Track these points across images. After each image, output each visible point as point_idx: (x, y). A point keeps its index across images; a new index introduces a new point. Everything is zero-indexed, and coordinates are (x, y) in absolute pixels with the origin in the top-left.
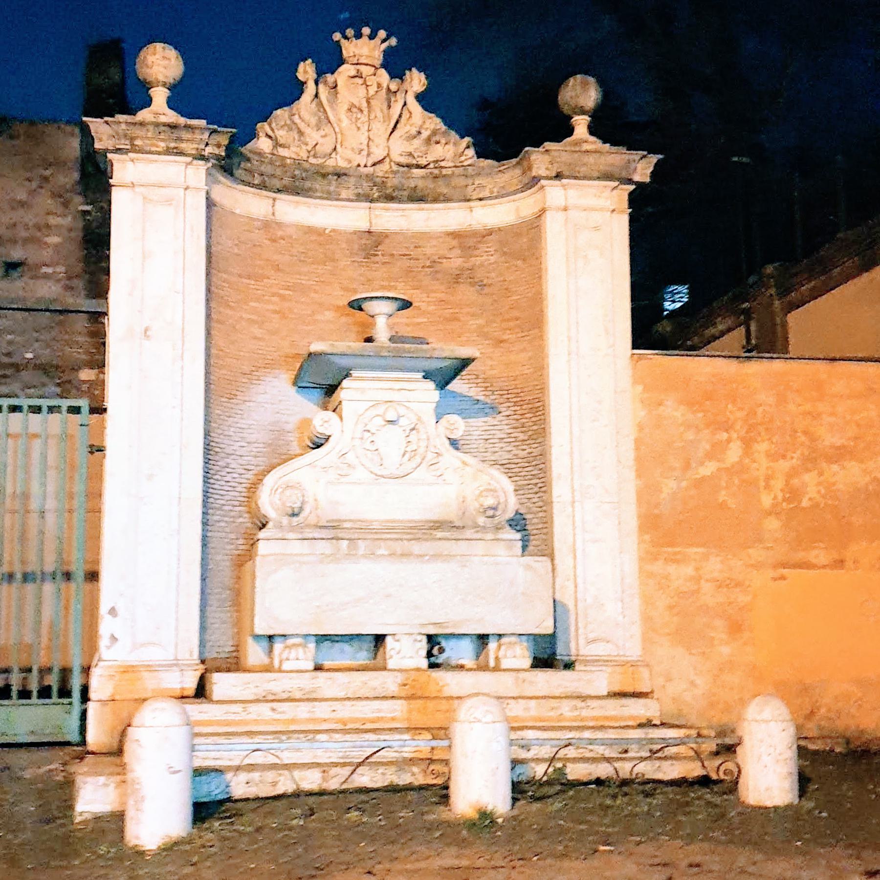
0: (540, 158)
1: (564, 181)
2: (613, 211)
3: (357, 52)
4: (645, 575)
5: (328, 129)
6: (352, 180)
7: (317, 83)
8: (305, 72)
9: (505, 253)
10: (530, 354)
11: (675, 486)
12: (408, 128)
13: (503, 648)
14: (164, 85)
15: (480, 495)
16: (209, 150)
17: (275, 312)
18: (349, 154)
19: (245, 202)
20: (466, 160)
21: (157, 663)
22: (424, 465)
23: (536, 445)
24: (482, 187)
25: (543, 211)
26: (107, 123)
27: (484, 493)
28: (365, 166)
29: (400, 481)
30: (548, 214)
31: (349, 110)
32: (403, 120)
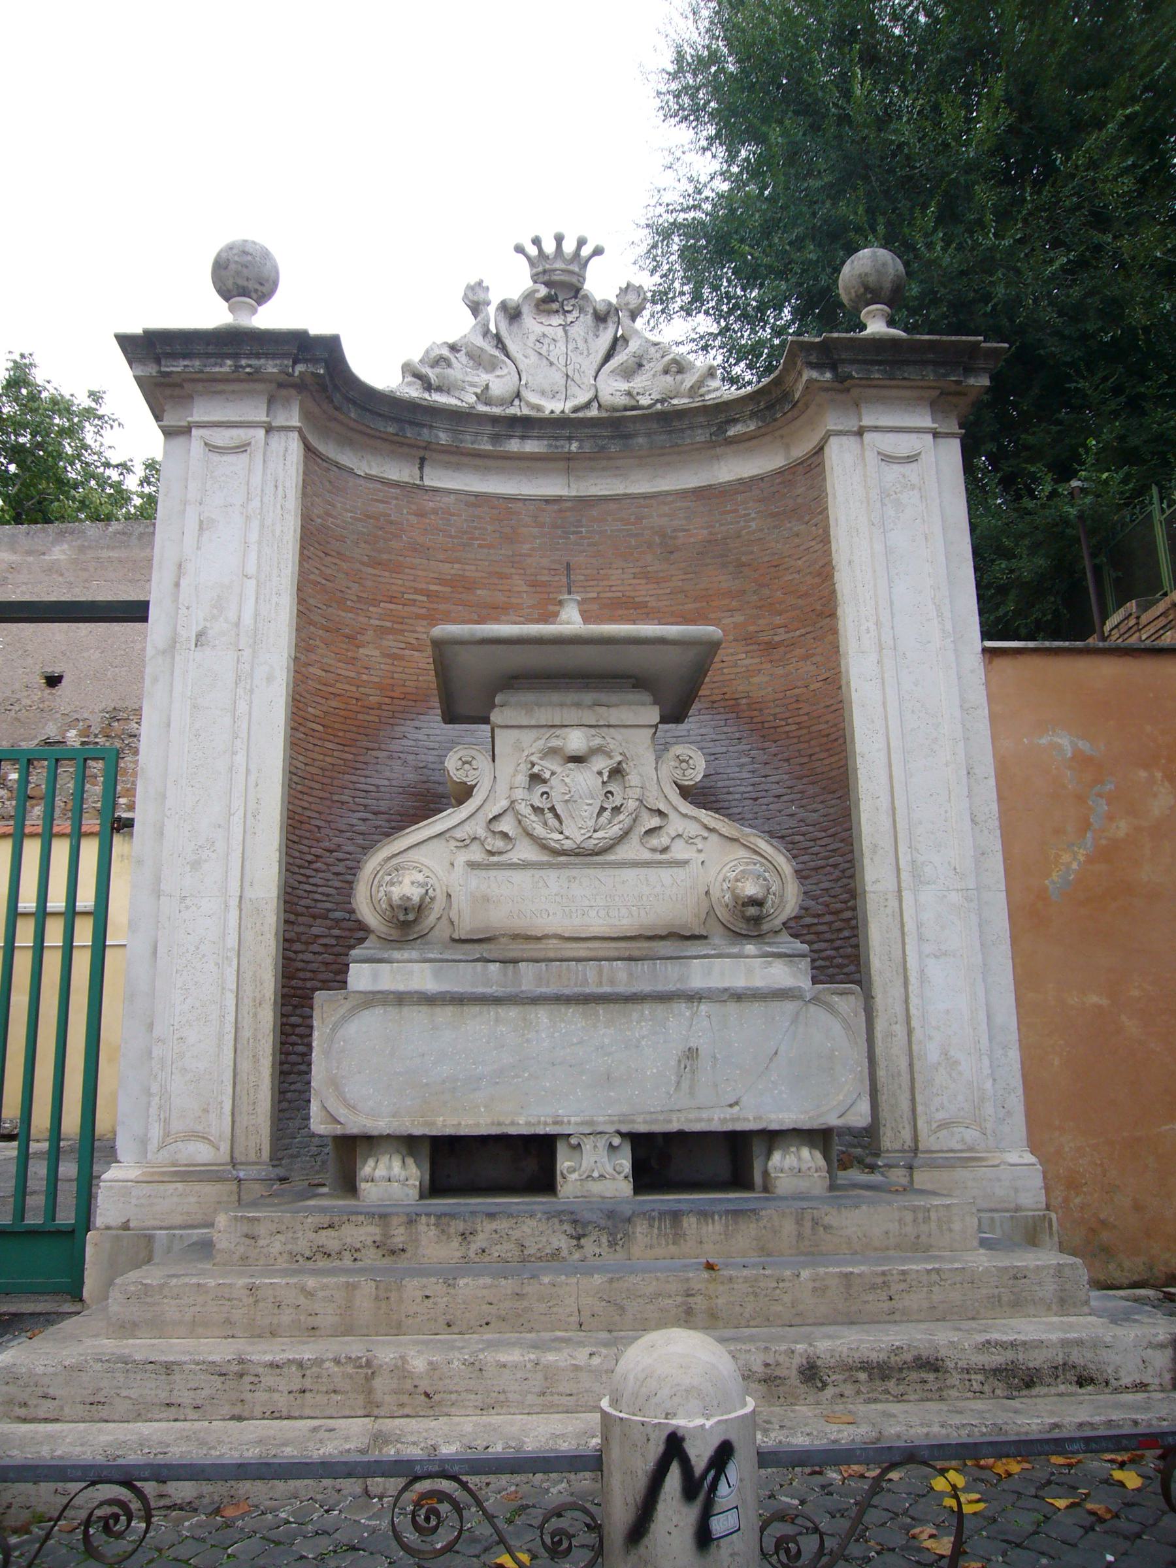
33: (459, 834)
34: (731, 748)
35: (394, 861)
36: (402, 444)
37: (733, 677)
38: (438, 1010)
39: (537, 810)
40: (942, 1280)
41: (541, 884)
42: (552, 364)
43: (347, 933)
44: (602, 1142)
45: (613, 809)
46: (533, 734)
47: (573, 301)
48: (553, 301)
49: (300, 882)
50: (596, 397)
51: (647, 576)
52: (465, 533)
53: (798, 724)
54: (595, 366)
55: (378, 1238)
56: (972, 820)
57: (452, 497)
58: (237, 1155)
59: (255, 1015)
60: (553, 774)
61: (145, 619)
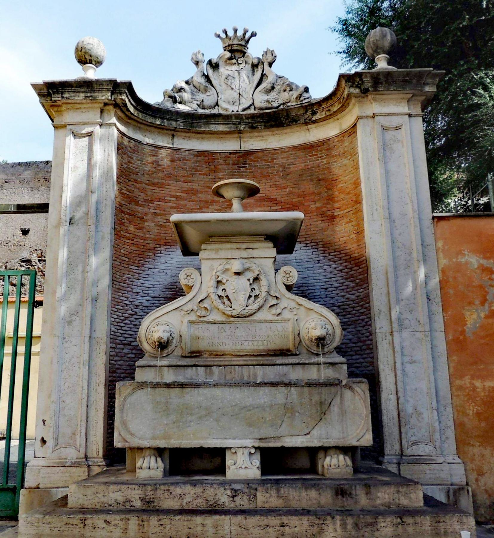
20: (305, 99)
23: (362, 290)
33: (185, 308)
34: (315, 265)
35: (156, 321)
36: (163, 129)
37: (316, 232)
38: (171, 390)
39: (220, 297)
40: (403, 522)
41: (222, 331)
42: (232, 89)
44: (246, 451)
45: (255, 296)
46: (219, 262)
47: (242, 59)
48: (233, 59)
49: (118, 329)
50: (253, 103)
51: (276, 186)
52: (193, 168)
53: (346, 253)
54: (253, 90)
55: (141, 496)
56: (428, 298)
57: (187, 152)
58: (88, 454)
60: (227, 280)
61: (47, 212)
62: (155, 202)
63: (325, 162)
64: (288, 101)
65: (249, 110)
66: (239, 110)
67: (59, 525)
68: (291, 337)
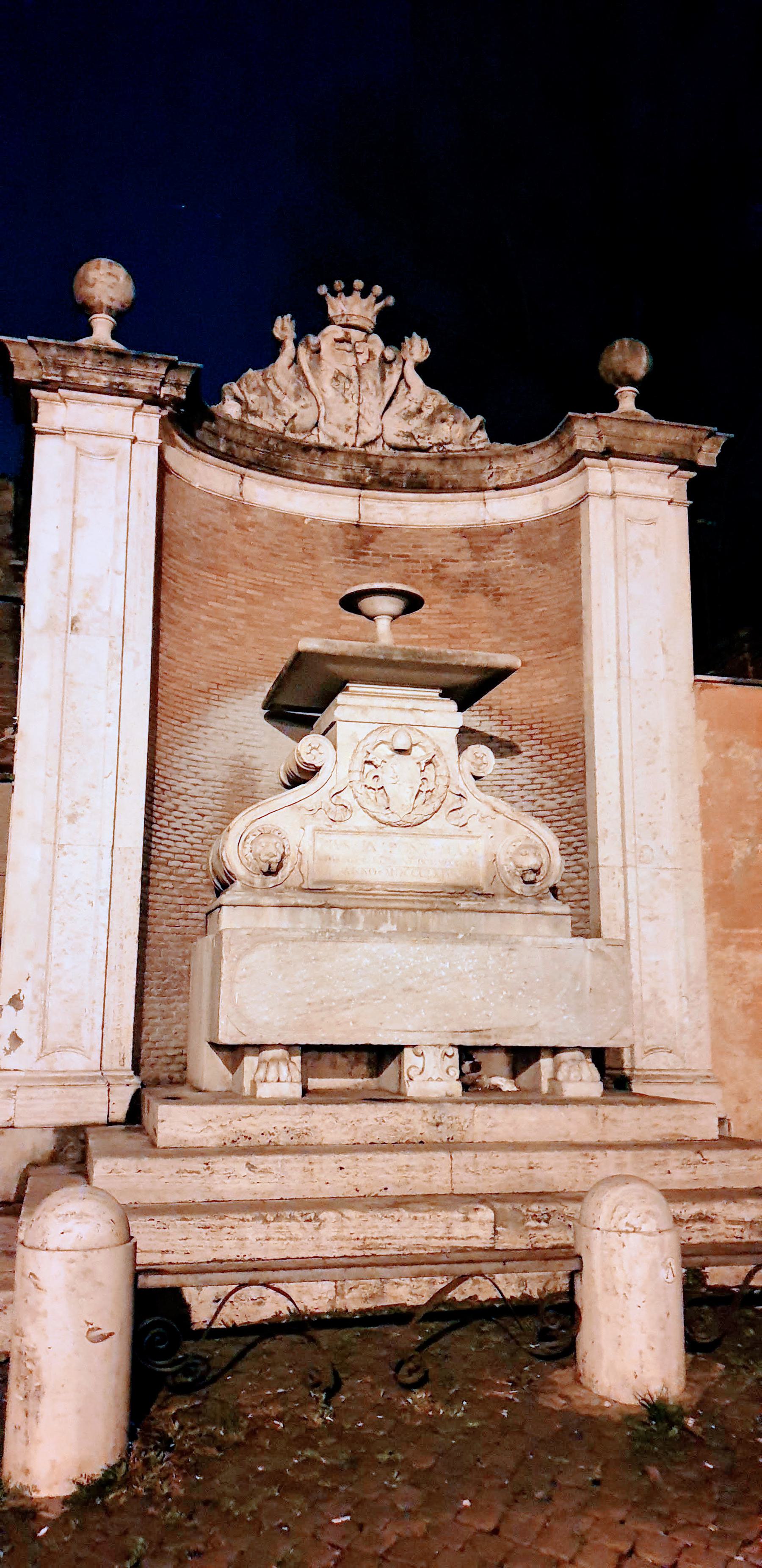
0: (585, 433)
1: (613, 460)
2: (670, 502)
3: (346, 311)
4: (715, 964)
5: (308, 399)
6: (341, 458)
7: (296, 343)
8: (283, 329)
9: (528, 556)
10: (562, 679)
11: (749, 850)
12: (407, 403)
13: (564, 1068)
14: (109, 310)
15: (517, 852)
16: (165, 390)
17: (241, 616)
18: (333, 431)
19: (207, 475)
21: (73, 1075)
22: (442, 812)
24: (501, 472)
25: (584, 497)
26: (31, 344)
27: (523, 851)
28: (354, 446)
29: (414, 830)
30: (591, 500)
31: (336, 379)
32: (399, 396)
33: (307, 804)
43: (180, 879)
50: (381, 434)
54: (383, 409)
59: (122, 946)
62: (210, 603)
63: (511, 565)
64: (448, 440)
65: (374, 447)
66: (358, 445)
67: (167, 1173)
68: (482, 865)
